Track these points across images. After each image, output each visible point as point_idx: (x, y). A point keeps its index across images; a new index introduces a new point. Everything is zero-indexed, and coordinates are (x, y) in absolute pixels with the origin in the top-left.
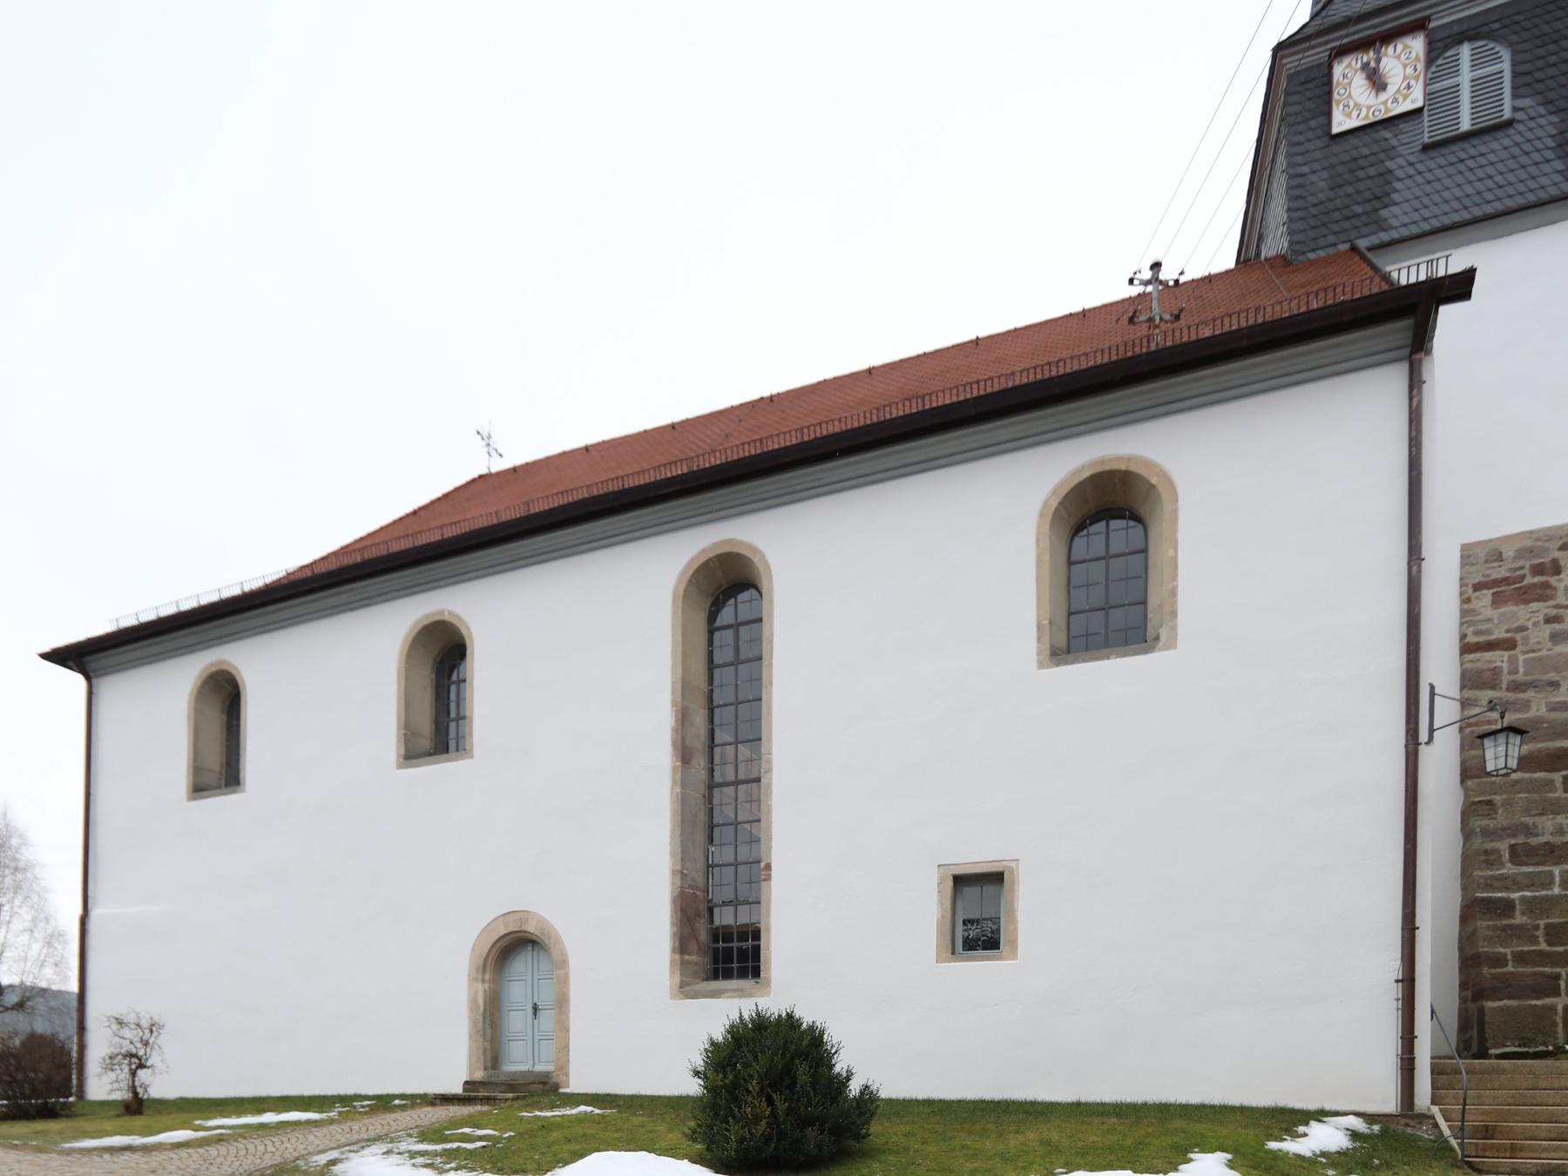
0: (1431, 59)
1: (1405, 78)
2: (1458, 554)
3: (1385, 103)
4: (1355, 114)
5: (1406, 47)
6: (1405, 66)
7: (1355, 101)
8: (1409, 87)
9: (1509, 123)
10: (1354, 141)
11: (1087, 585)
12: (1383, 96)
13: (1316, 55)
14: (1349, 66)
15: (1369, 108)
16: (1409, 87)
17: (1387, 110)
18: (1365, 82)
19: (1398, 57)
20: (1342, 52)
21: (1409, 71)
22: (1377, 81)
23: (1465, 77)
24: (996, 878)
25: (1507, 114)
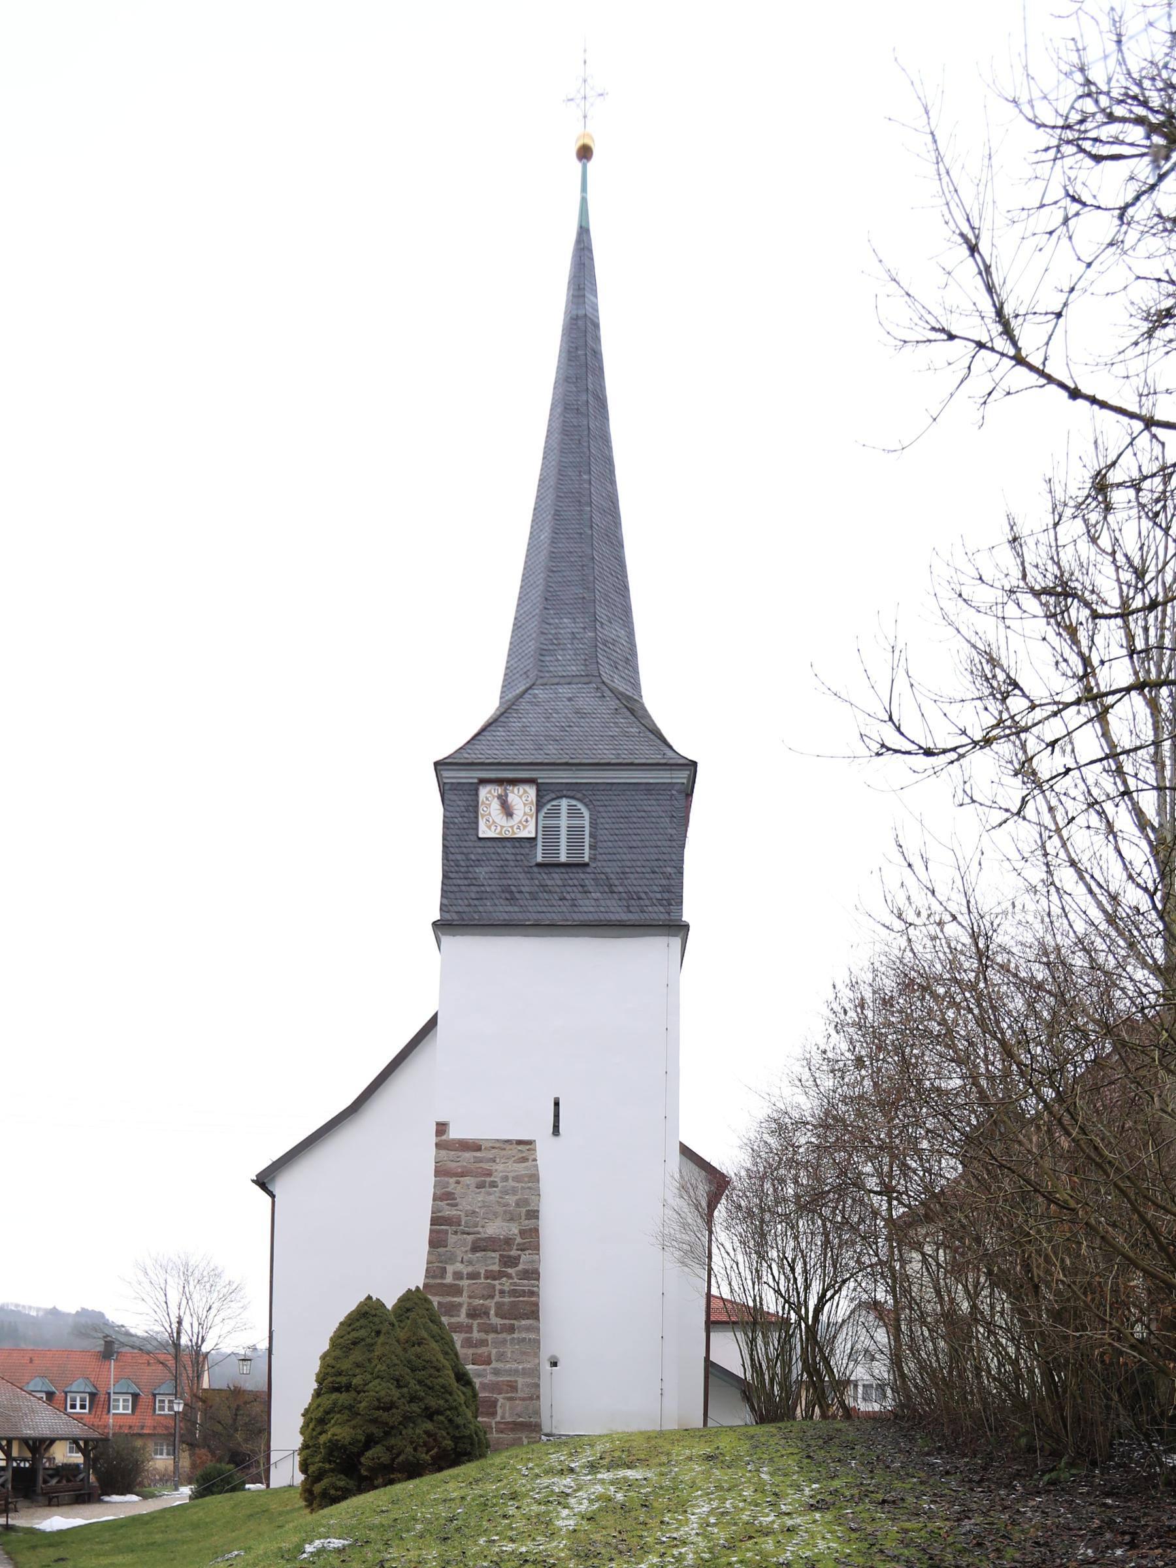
0: (539, 805)
1: (525, 814)
2: (352, 1306)
3: (512, 827)
4: (493, 828)
5: (525, 792)
6: (525, 805)
7: (492, 822)
8: (527, 821)
9: (586, 865)
10: (489, 844)
11: (1069, 734)
12: (511, 823)
13: (474, 775)
14: (490, 792)
15: (502, 827)
16: (527, 821)
17: (514, 833)
18: (499, 807)
19: (521, 797)
20: (484, 781)
21: (527, 810)
22: (508, 812)
23: (564, 822)
24: (256, 1182)
25: (586, 859)
